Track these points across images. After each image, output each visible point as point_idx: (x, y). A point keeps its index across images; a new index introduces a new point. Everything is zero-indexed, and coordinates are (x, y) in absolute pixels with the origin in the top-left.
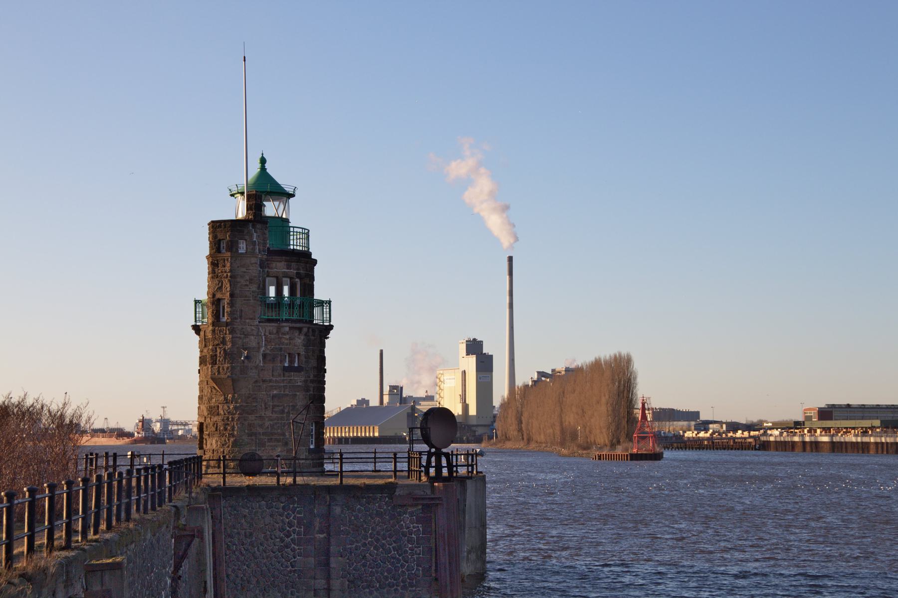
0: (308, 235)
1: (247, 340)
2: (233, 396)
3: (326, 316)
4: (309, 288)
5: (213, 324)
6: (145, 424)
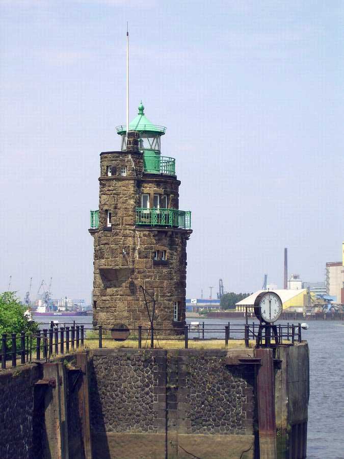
0: (174, 162)
3: (187, 223)
4: (176, 203)
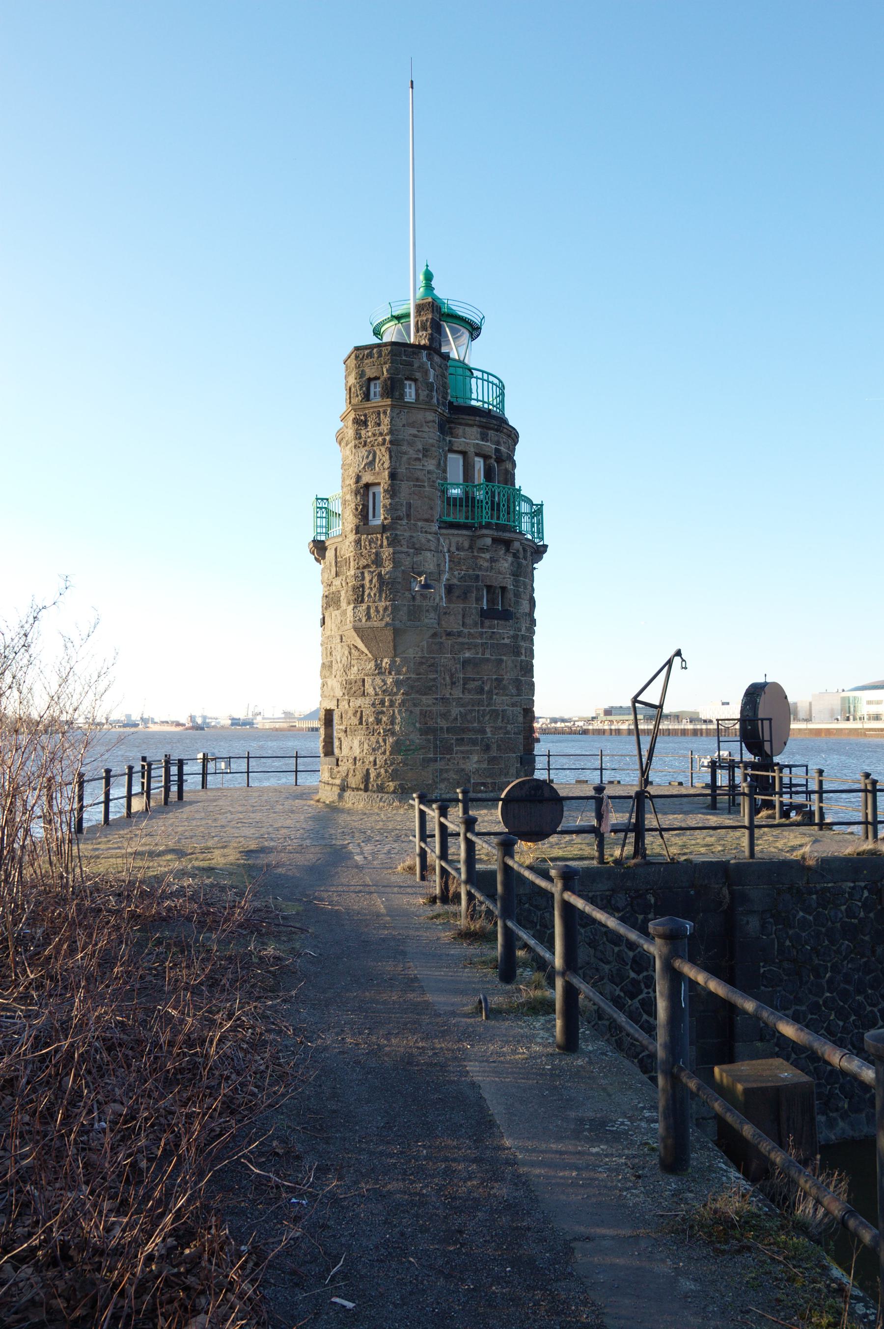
1: (420, 558)
2: (393, 662)
5: (358, 530)
6: (192, 719)
